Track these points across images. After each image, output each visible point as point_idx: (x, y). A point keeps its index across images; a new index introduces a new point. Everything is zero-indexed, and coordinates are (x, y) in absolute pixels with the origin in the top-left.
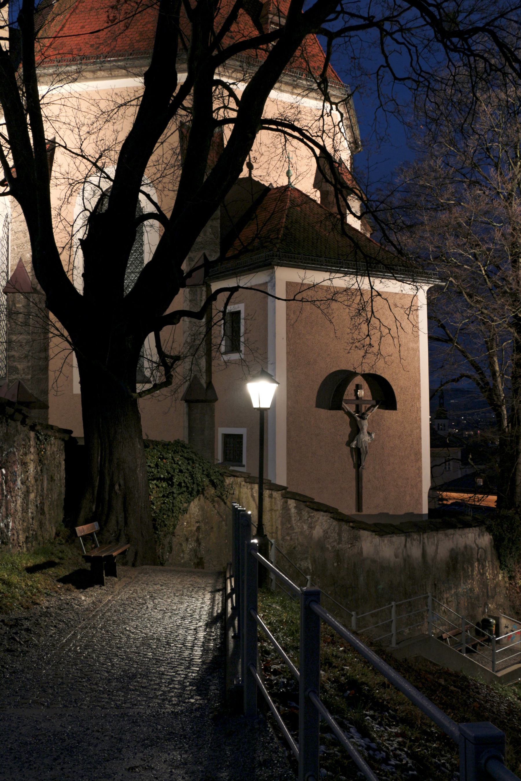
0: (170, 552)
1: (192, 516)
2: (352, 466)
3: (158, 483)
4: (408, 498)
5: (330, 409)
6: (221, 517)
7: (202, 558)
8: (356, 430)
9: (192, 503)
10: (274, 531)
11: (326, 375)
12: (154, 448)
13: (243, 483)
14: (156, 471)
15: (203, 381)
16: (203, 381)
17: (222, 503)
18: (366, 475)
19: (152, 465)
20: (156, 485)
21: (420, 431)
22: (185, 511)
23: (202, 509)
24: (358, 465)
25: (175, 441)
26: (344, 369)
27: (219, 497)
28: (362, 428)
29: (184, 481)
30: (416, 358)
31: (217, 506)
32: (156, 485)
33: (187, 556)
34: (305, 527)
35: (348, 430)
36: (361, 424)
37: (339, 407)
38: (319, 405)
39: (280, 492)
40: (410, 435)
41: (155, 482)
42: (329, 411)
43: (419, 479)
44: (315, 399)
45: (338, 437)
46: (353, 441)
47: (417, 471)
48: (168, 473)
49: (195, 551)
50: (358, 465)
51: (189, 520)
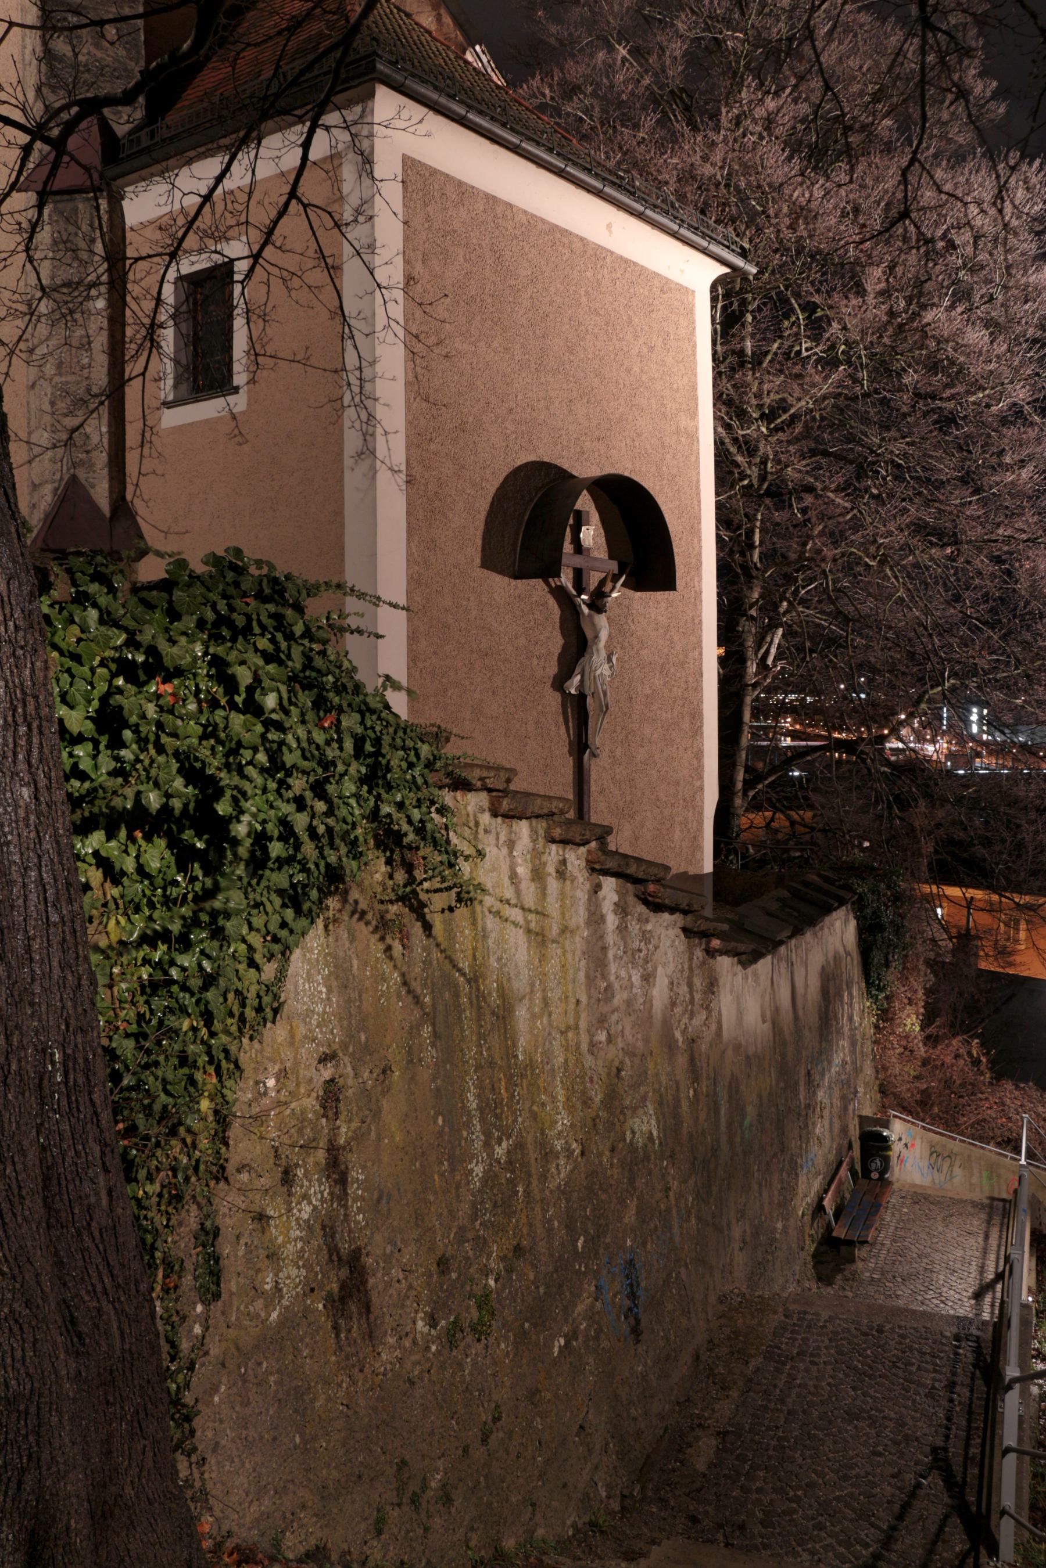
0: (211, 1293)
1: (301, 1030)
2: (566, 750)
3: (112, 849)
4: (677, 835)
5: (516, 578)
6: (417, 1000)
7: (356, 1255)
8: (577, 645)
9: (297, 955)
10: (571, 1022)
11: (506, 471)
12: (82, 599)
13: (485, 818)
14: (106, 763)
15: (101, 494)
16: (101, 494)
17: (417, 928)
18: (598, 771)
19: (76, 720)
20: (103, 862)
21: (701, 654)
22: (270, 1007)
23: (341, 977)
24: (580, 746)
25: (214, 560)
26: (546, 459)
27: (402, 899)
28: (597, 637)
29: (284, 822)
30: (693, 459)
31: (397, 948)
32: (103, 862)
33: (292, 1275)
34: (636, 979)
35: (556, 643)
36: (593, 625)
37: (548, 570)
38: (489, 562)
39: (583, 850)
40: (683, 664)
41: (96, 839)
42: (513, 582)
43: (698, 784)
44: (479, 542)
45: (535, 662)
46: (569, 675)
47: (695, 762)
48: (192, 773)
49: (327, 1228)
50: (580, 746)
51: (288, 1054)
